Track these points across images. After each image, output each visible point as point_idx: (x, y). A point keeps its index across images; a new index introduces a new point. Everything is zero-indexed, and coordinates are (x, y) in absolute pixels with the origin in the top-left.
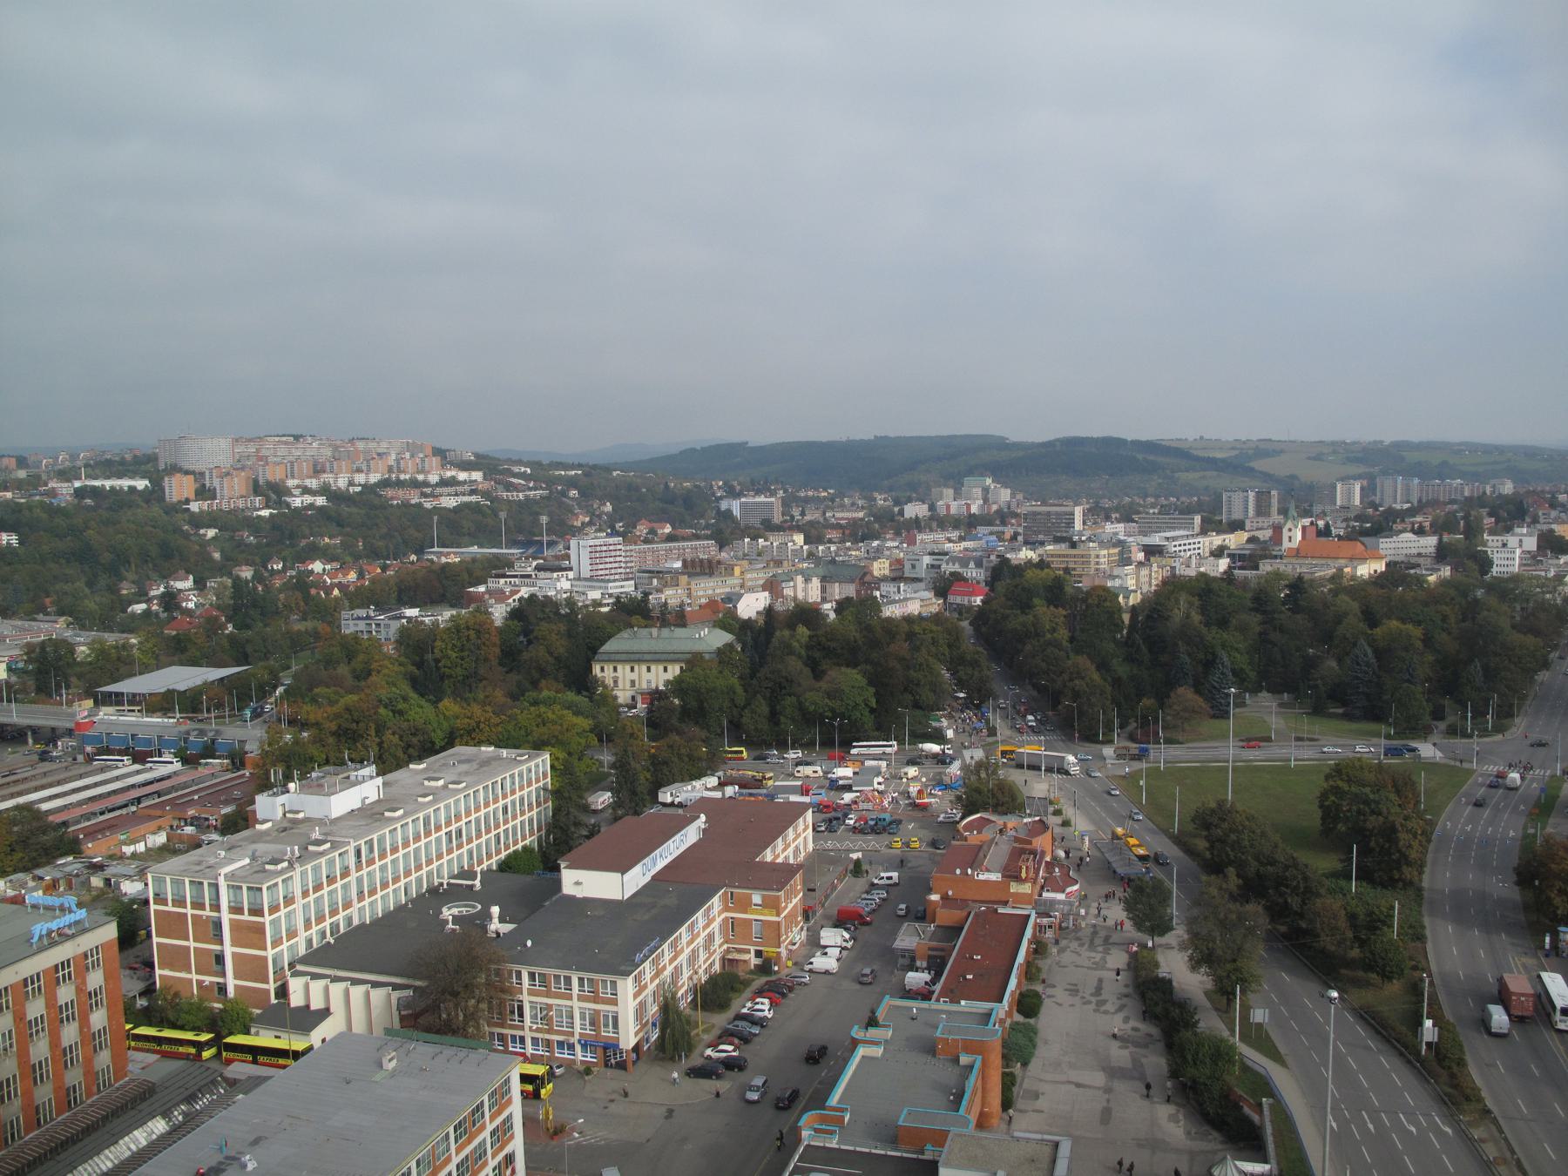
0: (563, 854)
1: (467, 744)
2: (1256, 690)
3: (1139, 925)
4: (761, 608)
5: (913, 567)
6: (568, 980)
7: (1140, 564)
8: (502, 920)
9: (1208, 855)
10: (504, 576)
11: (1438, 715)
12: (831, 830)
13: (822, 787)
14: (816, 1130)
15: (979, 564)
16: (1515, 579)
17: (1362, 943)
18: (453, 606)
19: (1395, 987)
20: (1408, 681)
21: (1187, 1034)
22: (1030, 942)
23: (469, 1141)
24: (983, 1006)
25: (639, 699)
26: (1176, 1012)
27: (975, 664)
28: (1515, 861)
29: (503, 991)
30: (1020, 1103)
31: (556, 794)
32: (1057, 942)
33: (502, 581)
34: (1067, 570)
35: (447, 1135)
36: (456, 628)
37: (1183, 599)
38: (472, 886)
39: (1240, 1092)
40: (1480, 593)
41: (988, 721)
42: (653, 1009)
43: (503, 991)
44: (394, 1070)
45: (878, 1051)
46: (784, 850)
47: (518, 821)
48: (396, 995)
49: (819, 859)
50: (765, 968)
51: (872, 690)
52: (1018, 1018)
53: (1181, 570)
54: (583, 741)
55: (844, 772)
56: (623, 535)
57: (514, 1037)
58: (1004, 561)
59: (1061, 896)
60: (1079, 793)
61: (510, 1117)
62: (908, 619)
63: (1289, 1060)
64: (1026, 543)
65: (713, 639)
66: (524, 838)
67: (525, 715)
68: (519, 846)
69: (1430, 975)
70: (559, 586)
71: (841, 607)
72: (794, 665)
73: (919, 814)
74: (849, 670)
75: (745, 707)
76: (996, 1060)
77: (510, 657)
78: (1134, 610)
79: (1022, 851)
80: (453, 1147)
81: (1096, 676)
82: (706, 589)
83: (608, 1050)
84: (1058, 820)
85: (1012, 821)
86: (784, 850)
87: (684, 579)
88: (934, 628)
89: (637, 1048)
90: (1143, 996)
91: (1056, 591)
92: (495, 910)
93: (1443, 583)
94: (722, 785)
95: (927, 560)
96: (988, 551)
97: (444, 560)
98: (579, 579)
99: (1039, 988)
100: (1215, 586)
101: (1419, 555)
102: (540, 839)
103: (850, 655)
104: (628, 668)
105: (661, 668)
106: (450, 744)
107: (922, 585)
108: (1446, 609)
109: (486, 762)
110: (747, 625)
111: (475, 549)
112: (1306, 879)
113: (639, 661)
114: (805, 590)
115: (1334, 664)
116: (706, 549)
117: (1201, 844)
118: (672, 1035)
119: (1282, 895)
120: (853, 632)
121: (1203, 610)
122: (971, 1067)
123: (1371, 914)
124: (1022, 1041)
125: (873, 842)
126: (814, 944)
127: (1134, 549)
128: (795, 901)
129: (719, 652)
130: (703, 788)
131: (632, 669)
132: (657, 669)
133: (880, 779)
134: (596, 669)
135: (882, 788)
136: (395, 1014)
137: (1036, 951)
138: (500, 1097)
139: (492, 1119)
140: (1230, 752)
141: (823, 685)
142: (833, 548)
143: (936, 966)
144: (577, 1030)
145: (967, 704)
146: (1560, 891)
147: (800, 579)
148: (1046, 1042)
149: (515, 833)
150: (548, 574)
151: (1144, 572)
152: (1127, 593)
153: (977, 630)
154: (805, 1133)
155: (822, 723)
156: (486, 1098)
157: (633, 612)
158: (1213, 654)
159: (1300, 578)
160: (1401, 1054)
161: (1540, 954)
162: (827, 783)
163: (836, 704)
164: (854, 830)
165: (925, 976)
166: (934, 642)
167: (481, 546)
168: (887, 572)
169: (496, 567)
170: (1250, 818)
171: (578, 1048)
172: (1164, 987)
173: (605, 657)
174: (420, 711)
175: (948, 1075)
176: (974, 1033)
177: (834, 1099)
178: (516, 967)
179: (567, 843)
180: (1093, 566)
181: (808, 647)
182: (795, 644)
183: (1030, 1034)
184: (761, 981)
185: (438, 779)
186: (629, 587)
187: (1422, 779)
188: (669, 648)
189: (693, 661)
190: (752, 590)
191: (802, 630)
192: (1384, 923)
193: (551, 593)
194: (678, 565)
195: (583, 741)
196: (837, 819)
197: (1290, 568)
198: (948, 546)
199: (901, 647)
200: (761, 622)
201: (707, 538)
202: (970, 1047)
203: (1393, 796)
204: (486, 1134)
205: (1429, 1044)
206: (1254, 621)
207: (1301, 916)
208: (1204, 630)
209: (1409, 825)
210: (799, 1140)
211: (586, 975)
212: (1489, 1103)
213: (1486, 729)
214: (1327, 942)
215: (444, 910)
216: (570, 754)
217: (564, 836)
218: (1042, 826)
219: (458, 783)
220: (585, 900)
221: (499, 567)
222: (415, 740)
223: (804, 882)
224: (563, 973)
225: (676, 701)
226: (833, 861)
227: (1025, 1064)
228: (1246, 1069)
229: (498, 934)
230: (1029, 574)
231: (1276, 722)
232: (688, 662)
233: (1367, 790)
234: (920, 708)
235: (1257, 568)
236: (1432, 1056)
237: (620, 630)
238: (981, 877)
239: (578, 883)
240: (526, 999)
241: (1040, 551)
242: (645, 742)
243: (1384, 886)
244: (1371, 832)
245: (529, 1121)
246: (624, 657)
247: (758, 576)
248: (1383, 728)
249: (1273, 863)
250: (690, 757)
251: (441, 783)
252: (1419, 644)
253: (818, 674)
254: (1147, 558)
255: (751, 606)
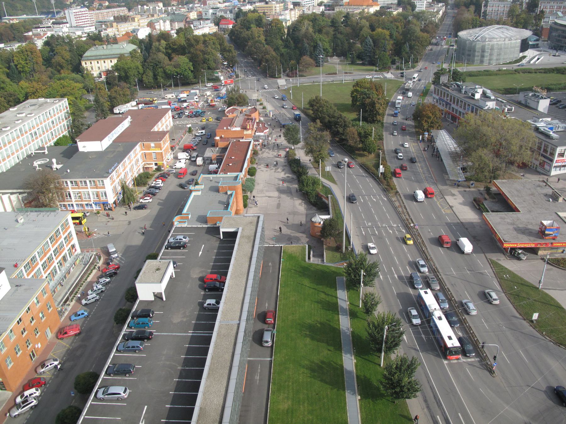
0: (77, 136)
1: (34, 98)
2: (332, 56)
3: (289, 142)
4: (147, 34)
5: (206, 14)
6: (85, 182)
7: (291, 9)
8: (58, 163)
9: (313, 116)
10: (39, 27)
11: (393, 62)
12: (179, 117)
13: (175, 102)
14: (179, 222)
15: (231, 12)
16: (423, 12)
17: (363, 142)
18: (19, 42)
19: (372, 155)
20: (384, 51)
21: (304, 177)
22: (252, 151)
23: (56, 242)
24: (235, 174)
25: (102, 74)
26: (301, 170)
27: (229, 51)
28: (413, 112)
29: (61, 189)
30: (250, 205)
31: (73, 114)
32: (261, 150)
33: (39, 30)
34: (264, 13)
35: (47, 242)
36: (21, 51)
37: (306, 22)
38: (44, 153)
39: (322, 194)
40: (410, 18)
41: (236, 73)
42: (119, 189)
43: (61, 189)
44: (23, 223)
45: (199, 193)
46: (162, 126)
47: (59, 126)
48: (20, 197)
49: (176, 128)
50: (158, 169)
51: (191, 63)
52: (249, 177)
53: (307, 12)
54: (80, 92)
55: (183, 96)
56: (88, 7)
57: (69, 205)
58: (240, 10)
59: (262, 134)
60: (269, 97)
61: (70, 232)
62: (204, 35)
63: (338, 182)
64: (249, 3)
65: (128, 48)
66: (62, 132)
67: (56, 84)
68: (61, 136)
69: (384, 152)
70: (64, 30)
71: (178, 32)
72: (162, 56)
73: (212, 108)
74: (182, 57)
75: (143, 74)
76: (240, 191)
77: (48, 61)
78: (289, 28)
79: (248, 118)
80: (50, 245)
81: (274, 53)
82: (125, 28)
83: (105, 204)
84: (261, 107)
85: (244, 109)
86: (162, 126)
87: (115, 24)
88: (214, 38)
89: (115, 203)
90: (290, 165)
91: (259, 22)
92: (54, 160)
93: (399, 14)
94: (138, 104)
95: (211, 11)
96: (234, 7)
97: (11, 22)
98: (71, 27)
99: (255, 166)
100: (318, 17)
101: (392, 4)
102: (69, 132)
103: (181, 50)
104: (96, 62)
105: (109, 61)
106: (26, 98)
107: (210, 21)
108: (398, 24)
109: (41, 105)
110: (142, 41)
111: (25, 16)
112: (345, 122)
113: (100, 59)
114: (164, 26)
115: (359, 46)
116: (123, 11)
117: (311, 112)
118: (126, 198)
119: (337, 128)
120: (183, 42)
121: (314, 27)
122: (231, 195)
123: (365, 132)
124: (249, 184)
125: (195, 120)
126: (176, 158)
127: (289, 4)
128: (167, 144)
129: (131, 53)
130: (131, 106)
131: (98, 63)
132: (108, 61)
133: (197, 97)
134: (83, 63)
135: (197, 100)
136: (22, 202)
137: (254, 153)
138: (65, 226)
139: (64, 234)
140: (322, 79)
141: (172, 63)
142: (174, 8)
143: (219, 161)
144: (92, 199)
145: (228, 66)
146: (426, 121)
147: (161, 21)
148: (258, 184)
149: (58, 131)
150: (58, 26)
151: (293, 12)
152: (286, 21)
153: (231, 37)
154: (176, 223)
155: (173, 77)
156: (59, 227)
157: (95, 39)
158: (316, 43)
159: (348, 13)
160: (373, 177)
161: (419, 142)
162: (177, 100)
163: (178, 70)
164: (188, 116)
165: (216, 166)
166: (214, 44)
167: (27, 15)
168: (196, 17)
169: (35, 24)
170: (326, 102)
171: (93, 205)
172: (297, 162)
173: (86, 58)
174: (11, 87)
175: (222, 197)
176: (232, 183)
177: (185, 211)
178: (64, 180)
179: (80, 132)
180: (274, 11)
181: (166, 49)
182: (161, 48)
183: (253, 182)
184: (158, 174)
185: (22, 113)
186: (93, 29)
187: (386, 86)
188: (111, 53)
189: (121, 57)
190: (143, 27)
191: (163, 42)
192: (369, 135)
193: (61, 34)
194: (112, 18)
195: (80, 92)
196: (182, 113)
197: (344, 10)
198: (219, 5)
199: (201, 46)
200: (147, 40)
201: (123, 6)
202: (231, 188)
203: (375, 92)
204: (62, 239)
205: (381, 173)
206: (331, 30)
207: (343, 134)
208: (313, 34)
209: (379, 101)
210: (172, 224)
211: (92, 180)
212: (398, 190)
213: (409, 67)
214: (351, 142)
215: (35, 163)
216: (76, 98)
217: (77, 130)
218: (255, 109)
219: (31, 114)
220: (89, 153)
221: (36, 24)
222: (11, 99)
223: (170, 137)
224: (83, 180)
225: (116, 74)
226: (181, 129)
227: (251, 192)
228: (323, 186)
229: (57, 169)
230: (250, 15)
231: (338, 67)
232: (119, 58)
233: (366, 90)
234: (211, 69)
235: (334, 10)
236: (382, 177)
237: (90, 47)
238: (233, 129)
239: (84, 147)
240: (71, 191)
241: (254, 6)
242: (106, 91)
243: (371, 123)
244: (366, 104)
245: (78, 233)
246: (94, 58)
247: (145, 21)
248: (374, 68)
249: (334, 117)
250: (124, 95)
251: (24, 115)
252: (388, 37)
253: (170, 59)
254: (294, 8)
255: (143, 34)
